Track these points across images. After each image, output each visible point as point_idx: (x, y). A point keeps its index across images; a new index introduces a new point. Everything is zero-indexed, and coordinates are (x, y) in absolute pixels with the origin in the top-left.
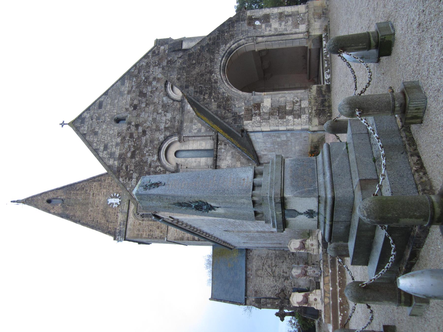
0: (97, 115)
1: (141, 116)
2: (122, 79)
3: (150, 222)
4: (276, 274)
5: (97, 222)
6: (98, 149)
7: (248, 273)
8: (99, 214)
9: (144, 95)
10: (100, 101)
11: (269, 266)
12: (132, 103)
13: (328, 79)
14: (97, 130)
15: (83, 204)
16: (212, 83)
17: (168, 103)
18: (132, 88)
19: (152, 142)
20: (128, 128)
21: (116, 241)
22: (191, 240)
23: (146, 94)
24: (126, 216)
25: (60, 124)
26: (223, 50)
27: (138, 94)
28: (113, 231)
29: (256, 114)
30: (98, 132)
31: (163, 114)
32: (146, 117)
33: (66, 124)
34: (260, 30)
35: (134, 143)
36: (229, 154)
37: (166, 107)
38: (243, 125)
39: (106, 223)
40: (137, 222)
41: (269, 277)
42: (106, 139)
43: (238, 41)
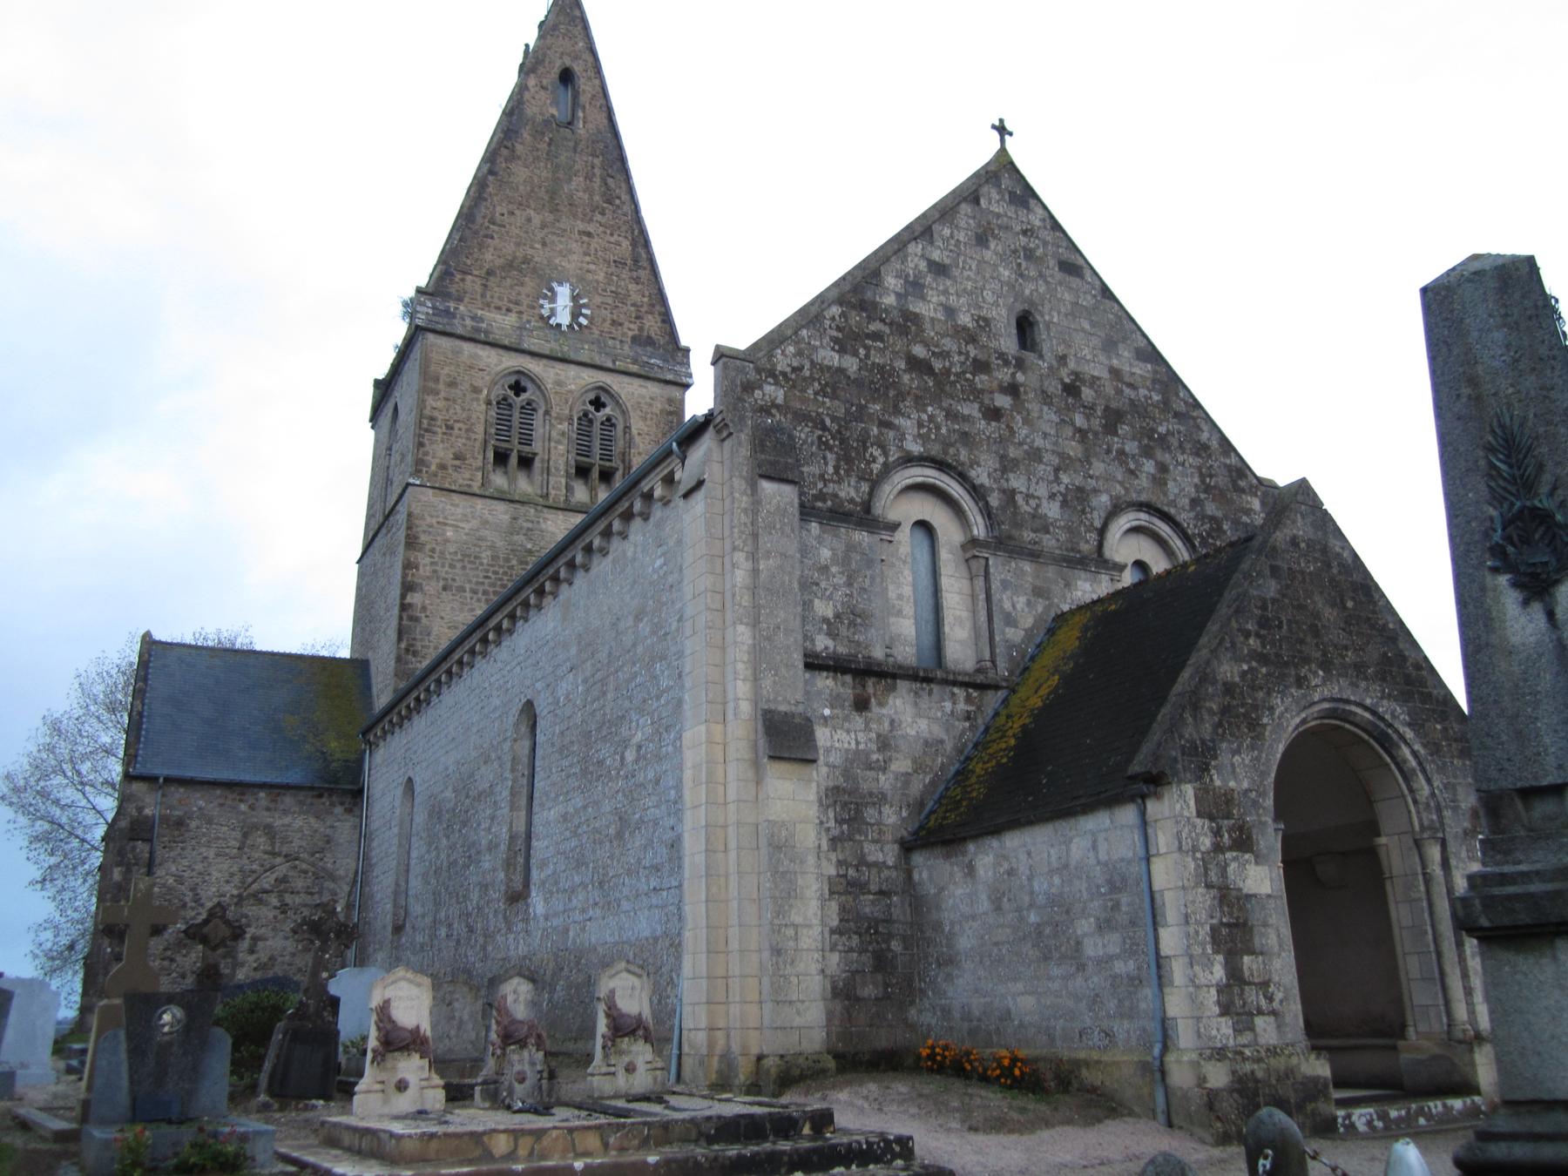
0: (1039, 252)
1: (1045, 408)
2: (1152, 355)
3: (480, 429)
4: (251, 910)
5: (486, 236)
6: (932, 243)
7: (262, 795)
8: (518, 244)
9: (1110, 428)
10: (1081, 267)
11: (283, 880)
12: (1083, 382)
13: (1352, 1125)
14: (992, 246)
15: (553, 194)
16: (1296, 667)
17: (1093, 509)
18: (1131, 385)
19: (965, 438)
20: (1002, 356)
21: (412, 293)
22: (404, 576)
23: (1115, 434)
24: (506, 342)
25: (1001, 121)
26: (1393, 716)
27: (1114, 405)
28: (453, 289)
29: (1217, 833)
30: (988, 248)
31: (1055, 488)
32: (1042, 427)
33: (1002, 141)
34: (1464, 854)
35: (957, 375)
36: (938, 732)
37: (1076, 499)
38: (1180, 782)
39: (481, 268)
40: (482, 381)
41: (237, 879)
42: (966, 274)
43: (1424, 771)
